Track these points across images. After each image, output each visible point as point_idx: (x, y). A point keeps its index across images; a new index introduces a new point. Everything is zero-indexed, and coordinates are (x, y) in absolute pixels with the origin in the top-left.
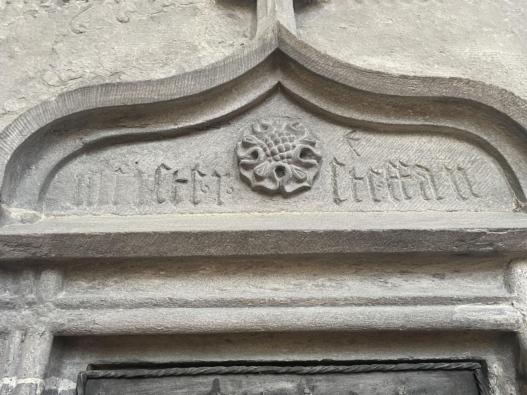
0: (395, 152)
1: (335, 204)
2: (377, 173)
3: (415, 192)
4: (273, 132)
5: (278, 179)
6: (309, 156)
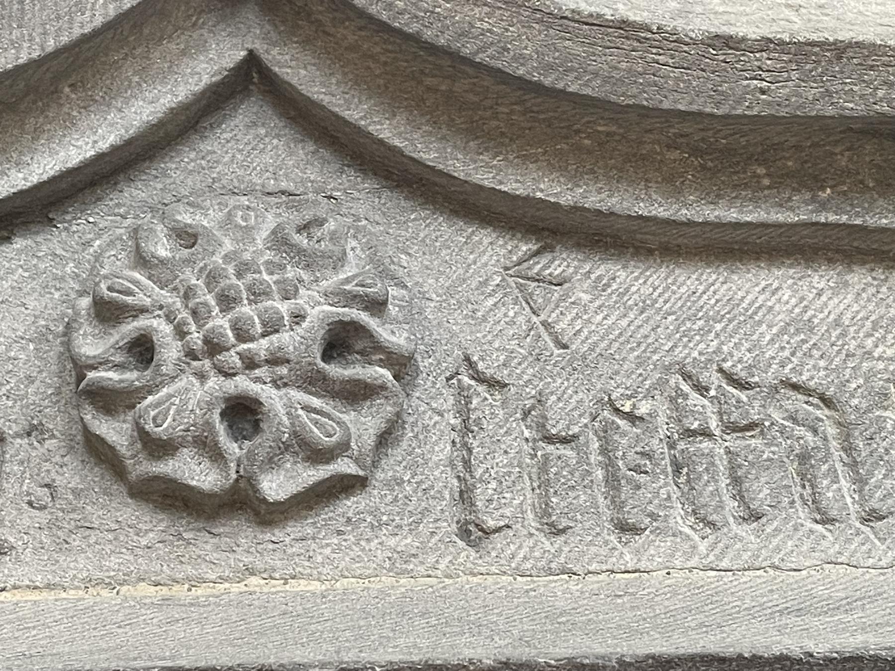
0: (704, 332)
1: (461, 544)
2: (632, 418)
3: (775, 494)
4: (218, 259)
5: (233, 449)
6: (361, 353)
